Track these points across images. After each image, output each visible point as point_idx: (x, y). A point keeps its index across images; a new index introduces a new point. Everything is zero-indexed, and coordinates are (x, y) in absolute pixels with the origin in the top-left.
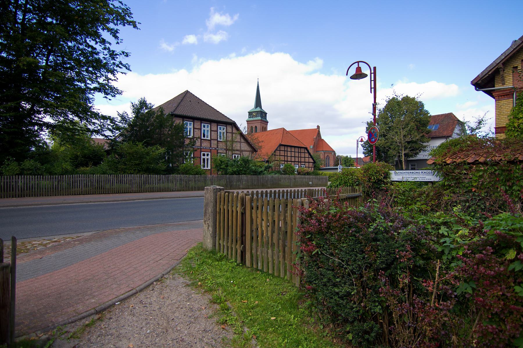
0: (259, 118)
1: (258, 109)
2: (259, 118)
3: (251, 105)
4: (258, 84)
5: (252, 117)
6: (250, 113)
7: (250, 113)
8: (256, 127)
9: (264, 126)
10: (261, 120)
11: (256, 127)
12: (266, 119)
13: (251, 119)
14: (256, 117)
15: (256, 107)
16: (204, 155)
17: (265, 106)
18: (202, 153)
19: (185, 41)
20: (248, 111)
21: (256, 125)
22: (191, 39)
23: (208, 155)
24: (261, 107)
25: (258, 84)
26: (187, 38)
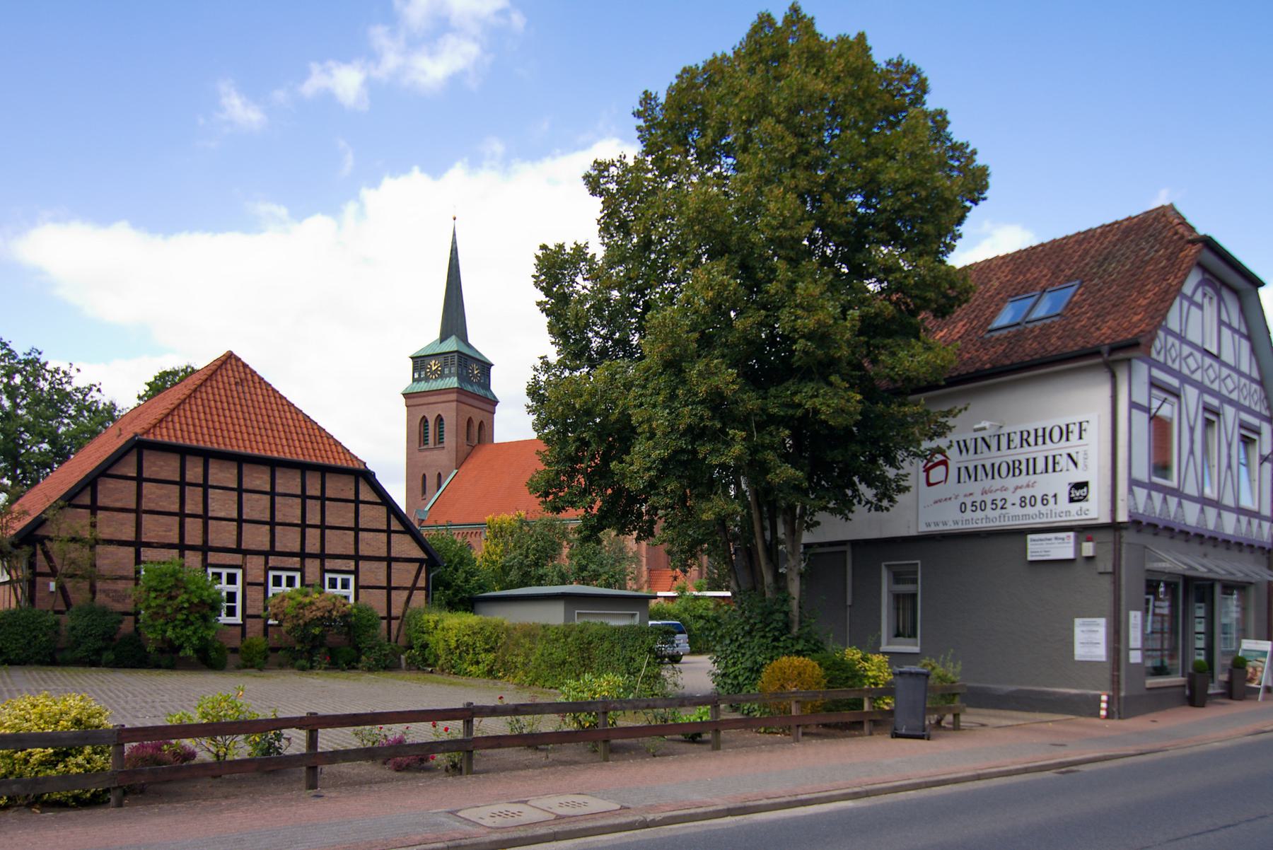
0: (453, 382)
1: (452, 345)
2: (453, 382)
3: (426, 332)
4: (454, 242)
5: (427, 379)
6: (419, 362)
7: (419, 362)
8: (440, 420)
9: (477, 416)
10: (459, 391)
11: (440, 420)
12: (487, 386)
13: (423, 386)
14: (442, 376)
15: (444, 338)
16: (277, 581)
17: (480, 338)
18: (271, 574)
19: (314, 83)
20: (412, 353)
21: (439, 410)
22: (347, 81)
23: (345, 585)
24: (463, 337)
25: (454, 242)
26: (327, 72)
